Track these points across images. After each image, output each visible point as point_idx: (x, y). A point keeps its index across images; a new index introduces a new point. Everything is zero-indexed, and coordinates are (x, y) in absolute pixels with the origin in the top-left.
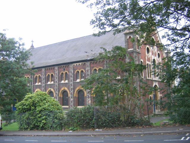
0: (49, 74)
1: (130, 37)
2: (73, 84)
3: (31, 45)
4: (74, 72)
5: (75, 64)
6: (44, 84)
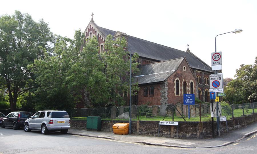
3: (187, 49)
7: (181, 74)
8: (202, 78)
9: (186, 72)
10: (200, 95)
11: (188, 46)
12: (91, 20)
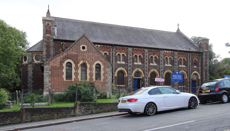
0: (181, 58)
1: (48, 24)
2: (163, 68)
3: (177, 29)
4: (164, 58)
5: (165, 51)
6: (131, 64)
7: (77, 55)
8: (174, 58)
9: (88, 51)
10: (185, 78)
11: (178, 25)
12: (177, 29)
